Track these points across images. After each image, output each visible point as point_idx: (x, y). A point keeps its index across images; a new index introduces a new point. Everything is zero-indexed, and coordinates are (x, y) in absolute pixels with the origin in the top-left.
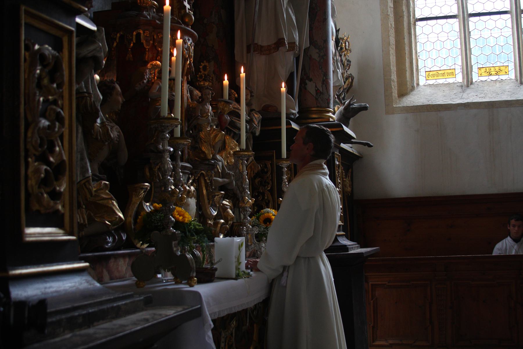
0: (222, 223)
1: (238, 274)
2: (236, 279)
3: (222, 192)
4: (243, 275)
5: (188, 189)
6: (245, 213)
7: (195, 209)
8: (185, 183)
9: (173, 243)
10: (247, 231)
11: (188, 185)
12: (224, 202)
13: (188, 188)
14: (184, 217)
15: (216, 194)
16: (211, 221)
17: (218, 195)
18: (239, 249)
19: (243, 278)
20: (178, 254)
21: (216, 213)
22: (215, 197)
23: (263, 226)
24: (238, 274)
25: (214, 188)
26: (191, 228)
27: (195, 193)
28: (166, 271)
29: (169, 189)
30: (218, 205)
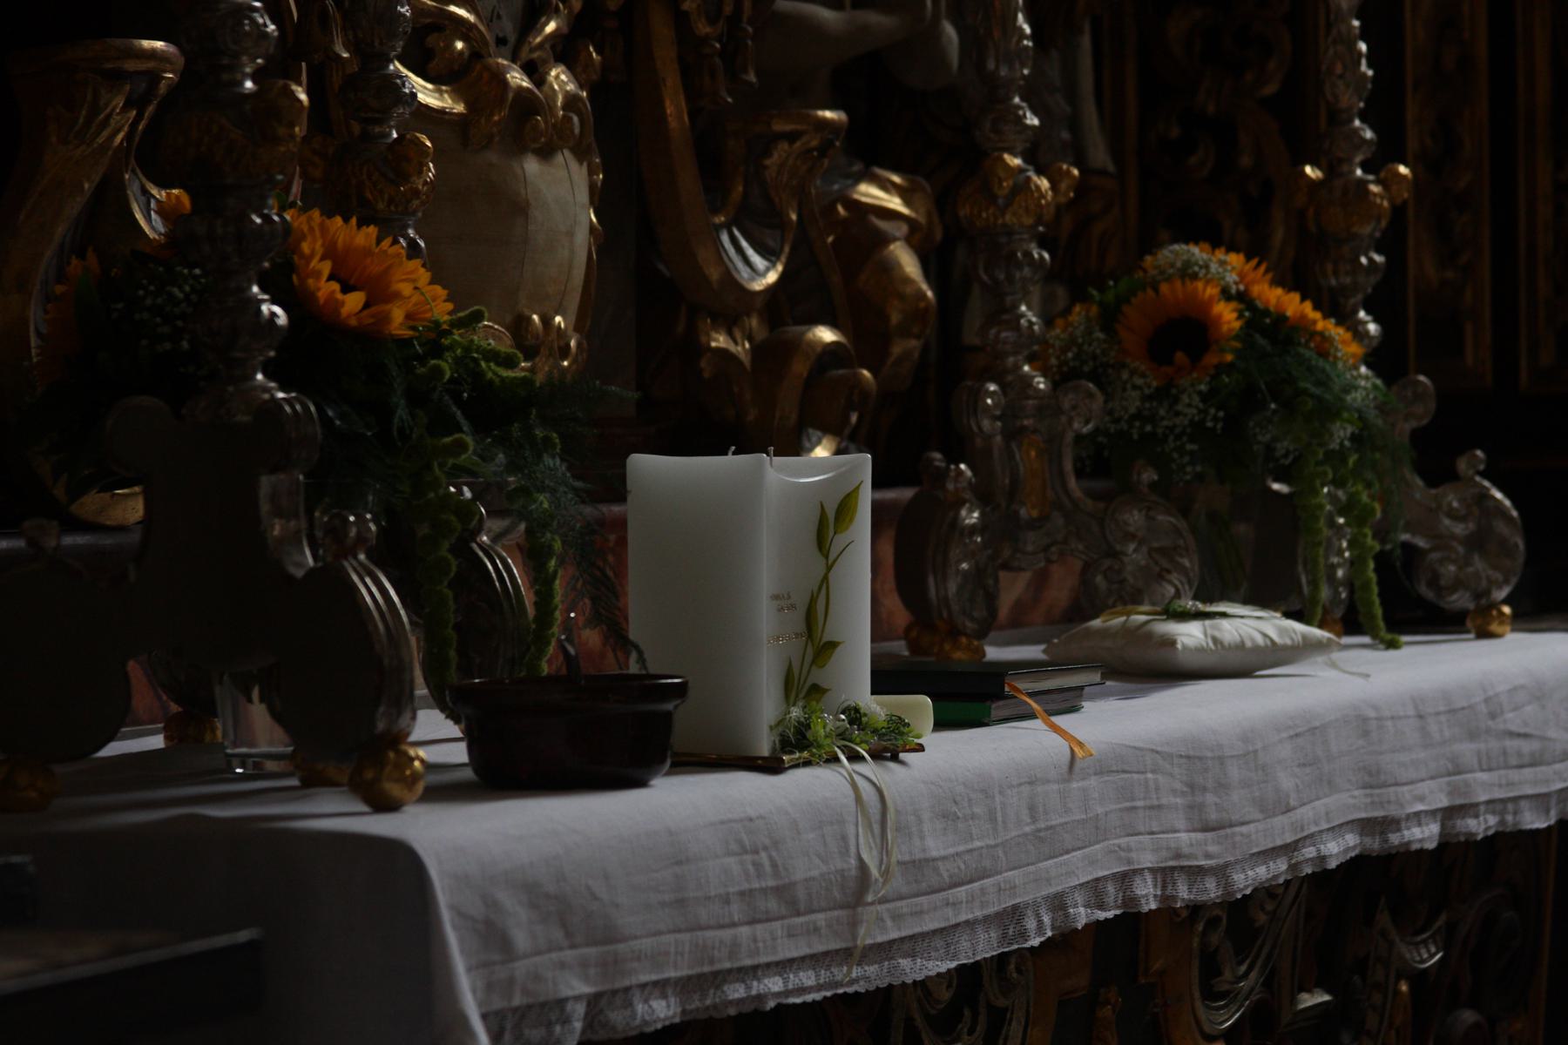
0: (819, 349)
1: (803, 729)
2: (772, 766)
3: (828, 114)
4: (842, 735)
5: (520, 88)
6: (1002, 277)
7: (582, 239)
8: (501, 41)
9: (266, 483)
10: (1009, 414)
11: (524, 54)
12: (869, 193)
13: (517, 78)
14: (378, 293)
15: (779, 126)
16: (730, 334)
17: (792, 137)
18: (822, 541)
19: (837, 760)
20: (299, 565)
21: (772, 277)
22: (767, 153)
23: (1139, 381)
24: (803, 729)
25: (752, 77)
26: (438, 371)
27: (576, 119)
28: (250, 701)
29: (241, 84)
30: (794, 217)
